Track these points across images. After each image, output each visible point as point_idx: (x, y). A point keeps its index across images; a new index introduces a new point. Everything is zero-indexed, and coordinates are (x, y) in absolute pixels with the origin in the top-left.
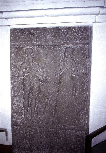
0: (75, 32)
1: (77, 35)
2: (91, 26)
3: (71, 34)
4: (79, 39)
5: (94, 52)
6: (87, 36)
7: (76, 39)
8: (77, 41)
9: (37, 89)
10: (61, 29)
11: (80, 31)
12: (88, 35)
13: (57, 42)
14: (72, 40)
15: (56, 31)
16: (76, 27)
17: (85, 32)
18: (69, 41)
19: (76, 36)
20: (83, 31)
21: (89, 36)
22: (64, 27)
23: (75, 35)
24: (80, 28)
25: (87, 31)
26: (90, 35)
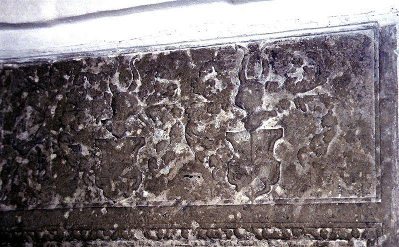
0: (220, 101)
1: (241, 125)
2: (382, 23)
3: (190, 123)
4: (265, 172)
5: (397, 15)
6: (350, 138)
7: (239, 175)
8: (240, 198)
9: (217, 129)
10: (92, 78)
11: (272, 87)
12: (361, 123)
13: (55, 203)
14: (198, 180)
15: (52, 99)
16: (230, 51)
17: (323, 99)
18: (162, 198)
19: (230, 137)
20: (304, 87)
21: (364, 136)
22: (120, 58)
23: (223, 129)
24: (274, 53)
25: (346, 79)
26: (380, 127)
